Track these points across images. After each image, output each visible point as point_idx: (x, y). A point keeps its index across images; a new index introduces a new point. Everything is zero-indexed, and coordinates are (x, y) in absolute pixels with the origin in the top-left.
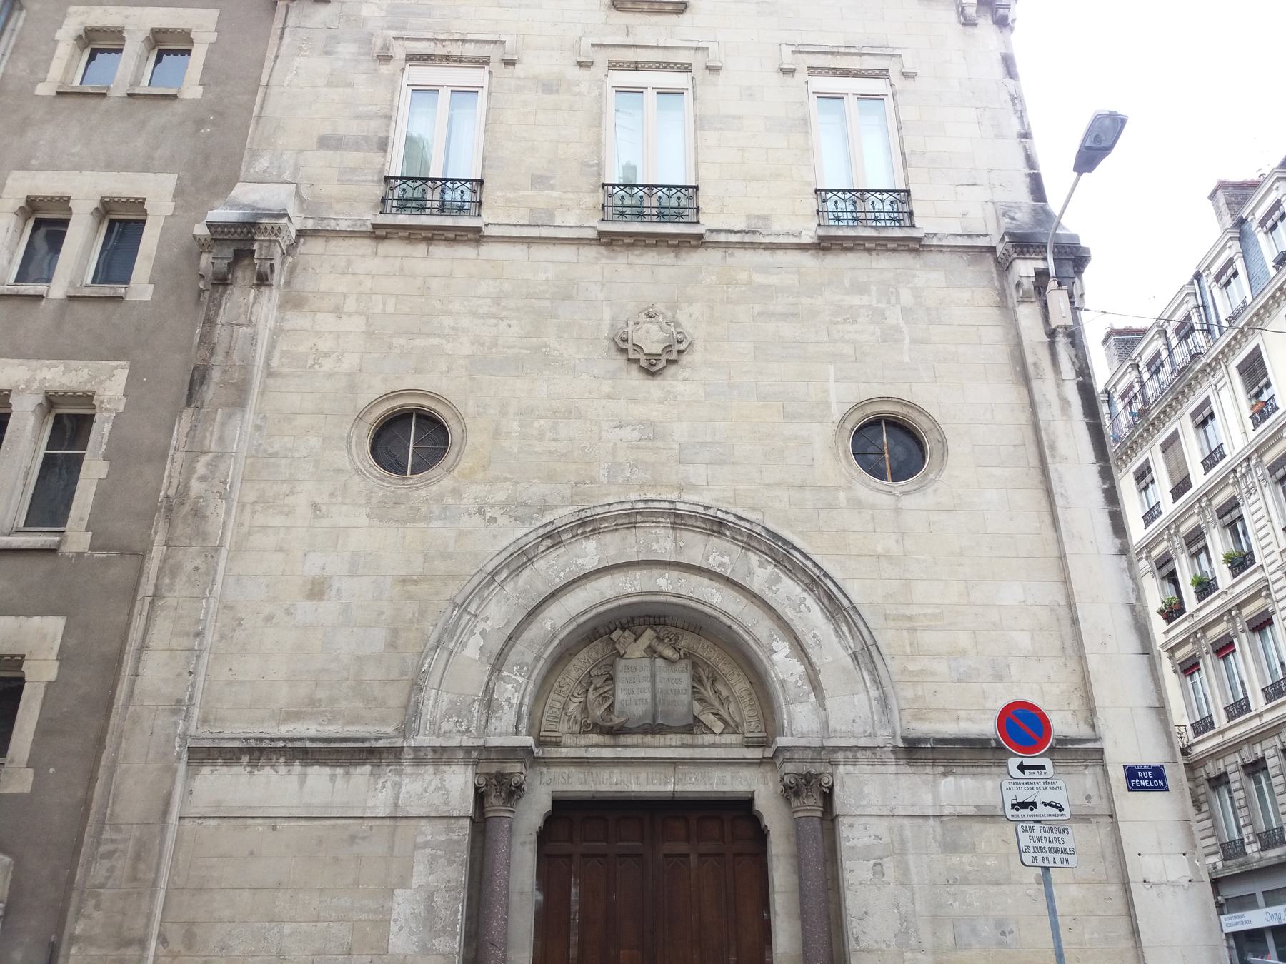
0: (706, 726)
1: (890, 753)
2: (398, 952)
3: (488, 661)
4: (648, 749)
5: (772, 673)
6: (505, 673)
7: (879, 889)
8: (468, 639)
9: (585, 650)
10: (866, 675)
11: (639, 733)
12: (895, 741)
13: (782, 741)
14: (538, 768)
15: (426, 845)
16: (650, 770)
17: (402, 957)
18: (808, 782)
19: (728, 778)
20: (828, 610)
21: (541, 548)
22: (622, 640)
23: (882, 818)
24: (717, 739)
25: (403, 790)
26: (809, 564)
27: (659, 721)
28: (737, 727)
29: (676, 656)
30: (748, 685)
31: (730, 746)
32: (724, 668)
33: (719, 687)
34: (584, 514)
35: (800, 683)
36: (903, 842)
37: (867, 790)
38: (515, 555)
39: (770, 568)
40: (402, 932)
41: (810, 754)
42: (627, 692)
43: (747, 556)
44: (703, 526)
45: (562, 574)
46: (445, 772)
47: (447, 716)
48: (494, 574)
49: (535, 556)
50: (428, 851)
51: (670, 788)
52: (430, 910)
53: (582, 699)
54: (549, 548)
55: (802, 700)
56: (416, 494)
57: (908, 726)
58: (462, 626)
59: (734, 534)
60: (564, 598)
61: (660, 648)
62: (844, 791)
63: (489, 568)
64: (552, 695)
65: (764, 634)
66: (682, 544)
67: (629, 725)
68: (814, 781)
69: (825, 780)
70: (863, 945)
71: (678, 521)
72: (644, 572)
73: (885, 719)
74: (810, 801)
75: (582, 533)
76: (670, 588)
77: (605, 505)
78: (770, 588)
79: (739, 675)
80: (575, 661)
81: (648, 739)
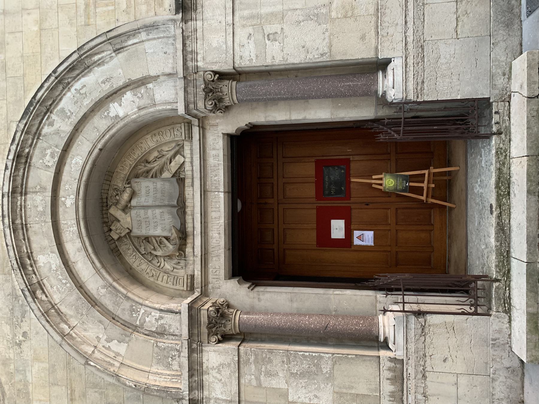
0: (179, 168)
1: (187, 25)
2: (331, 398)
4: (195, 211)
5: (133, 117)
6: (138, 323)
7: (286, 37)
8: (113, 352)
9: (127, 258)
10: (130, 42)
11: (185, 218)
12: (178, 20)
13: (181, 110)
14: (209, 291)
15: (258, 379)
16: (210, 209)
17: (335, 395)
18: (211, 91)
19: (213, 152)
20: (83, 71)
21: (44, 298)
22: (118, 231)
23: (235, 33)
24: (188, 160)
25: (220, 396)
26: (46, 85)
27: (175, 203)
28: (179, 145)
29: (128, 190)
30: (149, 136)
31: (191, 150)
32: (138, 154)
33: (151, 158)
34: (16, 266)
35: (140, 95)
36: (252, 17)
37: (215, 44)
38: (48, 318)
39: (53, 117)
40: (318, 395)
41: (191, 89)
42: (155, 227)
43: (45, 136)
44: (22, 171)
45: (64, 281)
46: (207, 367)
47: (168, 366)
48: (63, 335)
49: (51, 303)
50: (262, 378)
51: (222, 195)
52: (302, 375)
54: (44, 292)
55: (152, 94)
56: (8, 393)
57: (167, 10)
58: (103, 357)
59: (27, 145)
60: (82, 279)
61: (123, 202)
62: (216, 63)
63: (58, 338)
64: (159, 282)
66: (39, 187)
67: (178, 226)
68: (210, 87)
69: (209, 77)
70: (326, 50)
71: (19, 190)
72: (61, 217)
73: (162, 28)
74: (225, 90)
75: (32, 266)
76: (72, 196)
77: (8, 249)
78: (69, 118)
79: (141, 143)
80: (135, 266)
81: (188, 210)
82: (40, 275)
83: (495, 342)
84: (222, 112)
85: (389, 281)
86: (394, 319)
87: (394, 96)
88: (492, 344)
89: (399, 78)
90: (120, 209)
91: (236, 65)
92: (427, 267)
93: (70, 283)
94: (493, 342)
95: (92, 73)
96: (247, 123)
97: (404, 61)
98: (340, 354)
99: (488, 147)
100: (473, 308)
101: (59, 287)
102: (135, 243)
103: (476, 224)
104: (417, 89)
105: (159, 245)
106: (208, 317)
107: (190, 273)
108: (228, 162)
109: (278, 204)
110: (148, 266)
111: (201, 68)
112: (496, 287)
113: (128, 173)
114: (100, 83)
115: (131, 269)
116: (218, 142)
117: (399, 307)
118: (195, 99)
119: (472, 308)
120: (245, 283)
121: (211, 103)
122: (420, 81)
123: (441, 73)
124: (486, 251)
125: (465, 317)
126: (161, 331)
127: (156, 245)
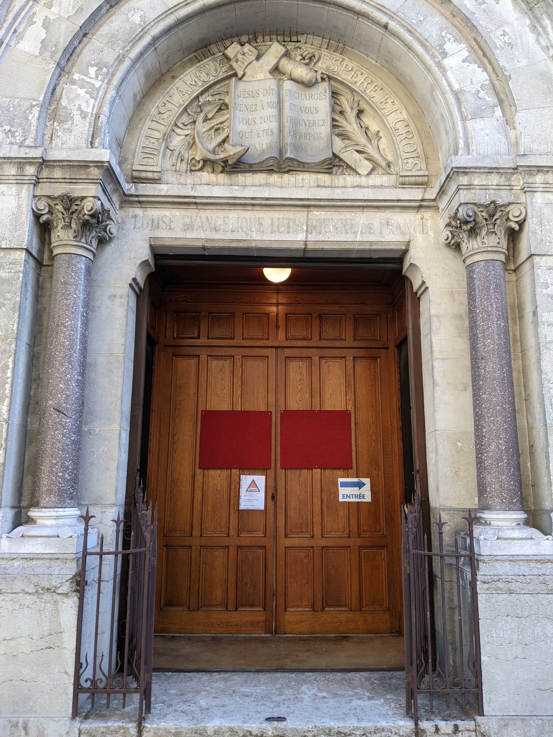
0: (348, 166)
3: (52, 57)
8: (25, 30)
14: (131, 210)
22: (240, 57)
28: (389, 166)
51: (301, 237)
55: (484, 115)
64: (148, 123)
69: (514, 212)
74: (492, 241)
80: (178, 83)
81: (275, 178)
83: (20, 727)
84: (447, 240)
85: (144, 528)
86: (71, 537)
87: (485, 539)
88: (17, 723)
89: (516, 549)
91: (537, 259)
92: (163, 601)
94: (20, 725)
95: (519, 15)
96: (427, 285)
97: (548, 558)
98: (7, 435)
99: (390, 713)
100: (88, 684)
102: (218, 86)
103: (243, 689)
104: (498, 581)
105: (213, 127)
106: (83, 198)
107: (165, 177)
108: (359, 251)
109: (276, 348)
111: (532, 198)
112: (128, 728)
113: (340, 79)
114: (503, 28)
115: (174, 78)
117: (94, 547)
118: (478, 187)
119: (89, 682)
120: (142, 279)
121: (471, 214)
122: (514, 586)
123: (528, 625)
124: (194, 708)
125: (71, 671)
126: (60, 115)
127: (214, 122)
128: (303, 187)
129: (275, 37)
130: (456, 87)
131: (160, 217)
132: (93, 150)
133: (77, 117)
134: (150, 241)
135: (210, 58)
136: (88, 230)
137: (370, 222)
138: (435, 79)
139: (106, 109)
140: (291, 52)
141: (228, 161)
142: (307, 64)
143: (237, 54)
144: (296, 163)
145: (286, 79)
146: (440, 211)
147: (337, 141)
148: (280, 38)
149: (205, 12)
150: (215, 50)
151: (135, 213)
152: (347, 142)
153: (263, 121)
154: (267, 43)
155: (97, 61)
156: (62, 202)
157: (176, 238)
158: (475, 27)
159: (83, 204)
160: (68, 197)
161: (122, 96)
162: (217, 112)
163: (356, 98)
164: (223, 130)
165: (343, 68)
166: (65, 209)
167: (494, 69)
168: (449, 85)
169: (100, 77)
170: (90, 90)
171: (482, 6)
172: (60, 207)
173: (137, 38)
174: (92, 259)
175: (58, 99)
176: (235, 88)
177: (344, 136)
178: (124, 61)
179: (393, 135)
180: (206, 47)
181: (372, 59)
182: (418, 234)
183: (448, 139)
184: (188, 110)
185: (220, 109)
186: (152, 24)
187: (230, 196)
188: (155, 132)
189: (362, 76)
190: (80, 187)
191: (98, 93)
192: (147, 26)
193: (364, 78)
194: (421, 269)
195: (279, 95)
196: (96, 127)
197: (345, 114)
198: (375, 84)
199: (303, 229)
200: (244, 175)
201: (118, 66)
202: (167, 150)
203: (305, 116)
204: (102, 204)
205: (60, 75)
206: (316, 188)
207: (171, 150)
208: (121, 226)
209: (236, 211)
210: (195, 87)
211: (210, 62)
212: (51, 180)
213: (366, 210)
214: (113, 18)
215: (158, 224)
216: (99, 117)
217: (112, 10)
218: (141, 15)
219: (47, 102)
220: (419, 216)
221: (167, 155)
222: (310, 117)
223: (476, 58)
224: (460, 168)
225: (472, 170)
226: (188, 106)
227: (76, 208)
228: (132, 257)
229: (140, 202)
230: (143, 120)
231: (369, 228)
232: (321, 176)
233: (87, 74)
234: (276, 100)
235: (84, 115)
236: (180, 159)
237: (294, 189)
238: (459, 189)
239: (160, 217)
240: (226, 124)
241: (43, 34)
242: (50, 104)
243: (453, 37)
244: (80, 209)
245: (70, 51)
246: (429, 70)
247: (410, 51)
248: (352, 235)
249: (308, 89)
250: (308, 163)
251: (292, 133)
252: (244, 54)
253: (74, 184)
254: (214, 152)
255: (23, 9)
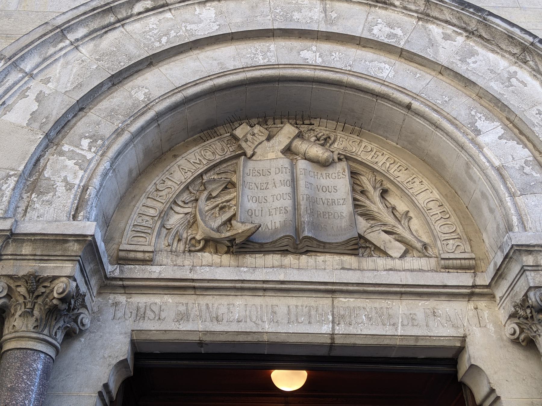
3: (40, 128)
8: (15, 103)
11: (274, 252)
14: (112, 296)
22: (249, 137)
28: (426, 248)
39: (460, 40)
45: (164, 40)
51: (326, 329)
53: (189, 210)
54: (147, 10)
58: (7, 85)
64: (143, 200)
65: (463, 113)
80: (181, 161)
81: (289, 259)
82: (178, 9)
84: (514, 334)
90: (291, 143)
93: (160, 47)
96: (498, 393)
101: (155, 32)
102: (225, 165)
105: (217, 206)
106: (55, 278)
110: (179, 183)
113: (360, 159)
115: (175, 156)
116: (443, 326)
126: (40, 186)
127: (219, 201)
128: (325, 269)
129: (286, 120)
130: (497, 163)
131: (148, 304)
132: (75, 223)
133: (61, 188)
134: (132, 335)
135: (216, 138)
136: (54, 318)
137: (411, 312)
138: (471, 156)
139: (96, 181)
140: (304, 134)
141: (235, 239)
142: (322, 145)
143: (247, 134)
144: (315, 242)
145: (299, 158)
146: (498, 299)
147: (361, 220)
148: (293, 122)
149: (214, 92)
150: (222, 131)
151: (116, 300)
152: (372, 222)
153: (275, 199)
154: (279, 126)
155: (92, 134)
156: (27, 283)
157: (165, 331)
158: (507, 106)
159: (52, 286)
160: (35, 277)
161: (116, 170)
162: (222, 190)
163: (378, 178)
164: (230, 207)
165: (362, 149)
166: (29, 292)
167: (534, 146)
168: (489, 161)
169: (93, 149)
170: (80, 161)
171: (510, 88)
172: (22, 290)
173: (139, 114)
174: (54, 357)
175: (40, 170)
176: (244, 167)
177: (368, 216)
178: (123, 134)
179: (426, 215)
180: (212, 128)
181: (392, 141)
182: (475, 328)
183: (495, 218)
184: (190, 188)
185: (226, 188)
186: (157, 101)
187: (237, 278)
188: (150, 209)
189: (383, 157)
190: (52, 265)
191: (89, 165)
192: (151, 102)
193: (385, 159)
194: (487, 372)
195: (293, 173)
196: (82, 199)
197: (367, 194)
198: (399, 164)
199: (328, 319)
200: (254, 256)
201: (115, 139)
202: (163, 229)
203: (322, 195)
204: (77, 286)
205: (47, 147)
206: (342, 271)
207: (167, 229)
208: (96, 317)
209: (244, 297)
210: (199, 166)
211: (217, 142)
212: (18, 257)
213: (404, 297)
214: (115, 94)
215: (144, 313)
216: (88, 188)
217: (114, 87)
218: (145, 93)
219: (27, 173)
220: (471, 305)
221: (162, 234)
222: (328, 196)
223: (513, 135)
224: (522, 245)
225: (536, 249)
226: (190, 183)
227: (43, 290)
228: (106, 356)
229: (124, 287)
230: (137, 197)
231: (412, 319)
232: (346, 258)
233: (78, 146)
234: (290, 178)
235: (69, 187)
236: (177, 239)
237: (314, 271)
238: (525, 271)
239: (148, 304)
240: (233, 202)
241: (35, 107)
242: (30, 175)
243: (484, 116)
244: (48, 292)
245: (63, 123)
246: (462, 147)
247: (438, 130)
248: (391, 327)
249: (324, 168)
250: (329, 243)
251: (309, 212)
252: (254, 135)
253: (44, 262)
254: (218, 230)
255: (17, 84)
